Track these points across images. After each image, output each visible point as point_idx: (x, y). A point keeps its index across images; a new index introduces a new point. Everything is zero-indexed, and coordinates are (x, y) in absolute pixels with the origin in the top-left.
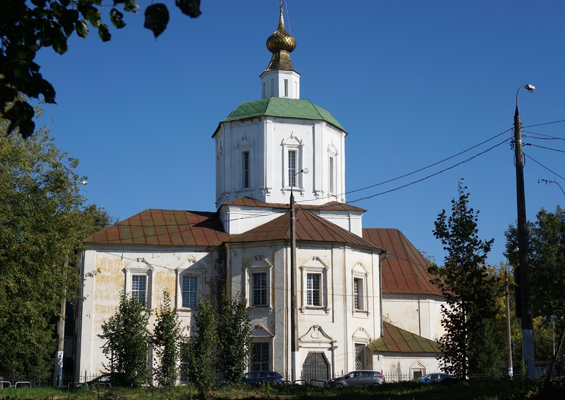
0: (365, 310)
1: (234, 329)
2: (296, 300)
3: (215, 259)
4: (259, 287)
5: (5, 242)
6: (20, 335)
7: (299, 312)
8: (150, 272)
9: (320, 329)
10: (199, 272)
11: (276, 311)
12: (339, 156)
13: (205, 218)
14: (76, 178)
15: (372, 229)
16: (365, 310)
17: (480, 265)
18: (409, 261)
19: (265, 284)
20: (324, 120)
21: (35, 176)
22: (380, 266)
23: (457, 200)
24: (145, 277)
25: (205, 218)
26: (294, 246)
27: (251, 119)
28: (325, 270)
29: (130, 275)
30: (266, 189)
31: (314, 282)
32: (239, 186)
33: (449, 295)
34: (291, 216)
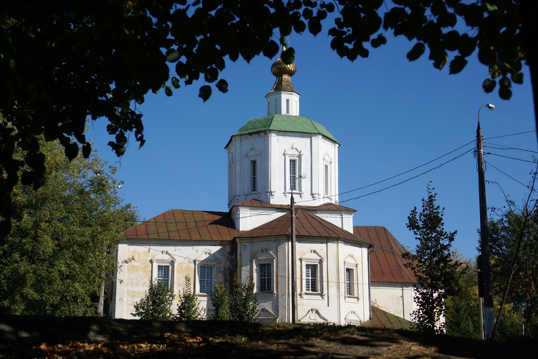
0: (356, 295)
1: (244, 307)
2: (296, 285)
3: (227, 252)
4: (265, 276)
5: (59, 234)
6: (69, 311)
7: (299, 297)
8: (172, 263)
9: (317, 312)
10: (214, 263)
11: (279, 296)
12: (333, 164)
13: (218, 217)
14: (114, 182)
15: (361, 227)
16: (356, 295)
17: (446, 252)
18: (393, 254)
19: (270, 274)
20: (320, 134)
21: (82, 181)
22: (368, 258)
23: (426, 199)
24: (168, 267)
25: (218, 217)
26: (294, 239)
27: (258, 133)
28: (321, 261)
29: (155, 265)
30: (271, 192)
31: (312, 271)
32: (248, 189)
33: (420, 276)
34: (292, 214)
